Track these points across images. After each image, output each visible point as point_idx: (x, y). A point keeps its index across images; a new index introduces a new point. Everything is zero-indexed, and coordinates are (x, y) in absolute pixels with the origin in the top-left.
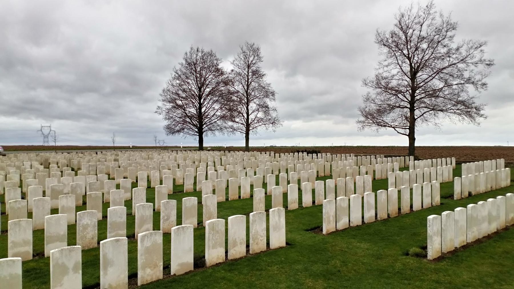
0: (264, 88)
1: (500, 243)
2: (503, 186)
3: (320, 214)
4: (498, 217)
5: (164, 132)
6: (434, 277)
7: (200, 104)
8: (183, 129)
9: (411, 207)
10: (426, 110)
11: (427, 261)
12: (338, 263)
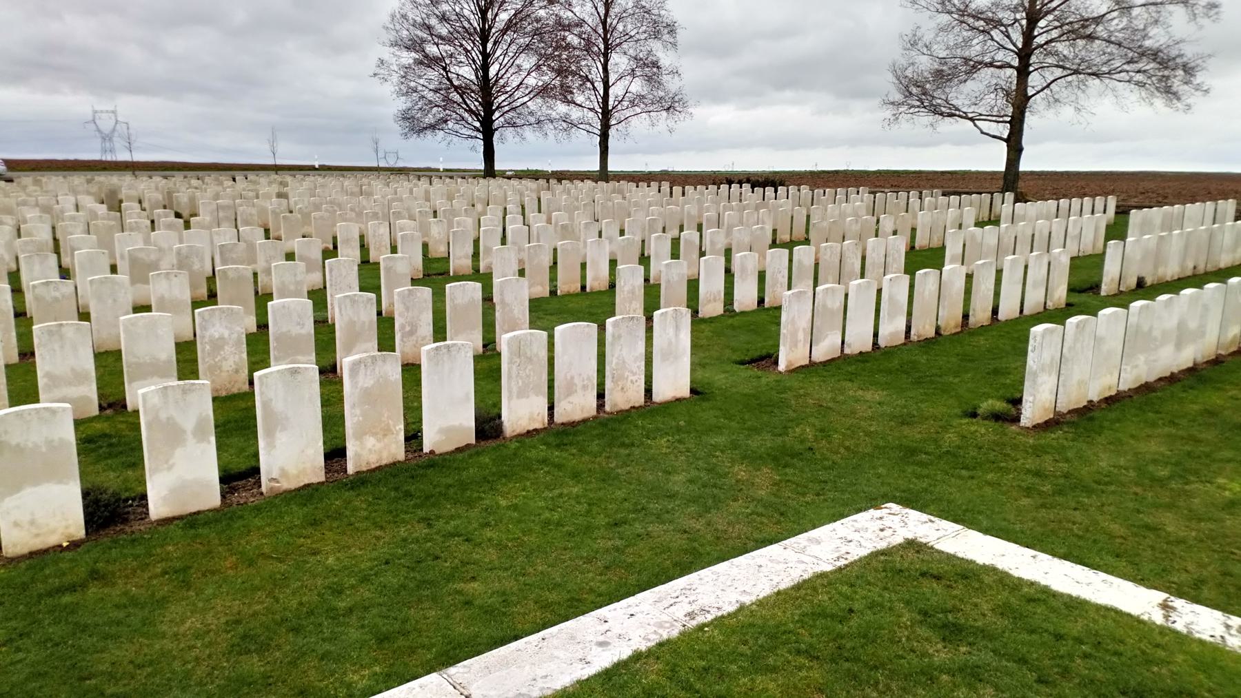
0: (648, 12)
1: (1195, 392)
2: (1222, 265)
3: (774, 328)
4: (1201, 332)
5: (397, 128)
6: (1031, 463)
7: (486, 56)
8: (446, 121)
9: (995, 311)
10: (1058, 72)
11: (1018, 430)
12: (809, 433)
